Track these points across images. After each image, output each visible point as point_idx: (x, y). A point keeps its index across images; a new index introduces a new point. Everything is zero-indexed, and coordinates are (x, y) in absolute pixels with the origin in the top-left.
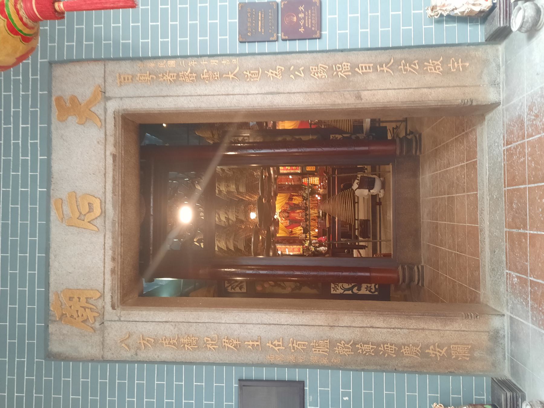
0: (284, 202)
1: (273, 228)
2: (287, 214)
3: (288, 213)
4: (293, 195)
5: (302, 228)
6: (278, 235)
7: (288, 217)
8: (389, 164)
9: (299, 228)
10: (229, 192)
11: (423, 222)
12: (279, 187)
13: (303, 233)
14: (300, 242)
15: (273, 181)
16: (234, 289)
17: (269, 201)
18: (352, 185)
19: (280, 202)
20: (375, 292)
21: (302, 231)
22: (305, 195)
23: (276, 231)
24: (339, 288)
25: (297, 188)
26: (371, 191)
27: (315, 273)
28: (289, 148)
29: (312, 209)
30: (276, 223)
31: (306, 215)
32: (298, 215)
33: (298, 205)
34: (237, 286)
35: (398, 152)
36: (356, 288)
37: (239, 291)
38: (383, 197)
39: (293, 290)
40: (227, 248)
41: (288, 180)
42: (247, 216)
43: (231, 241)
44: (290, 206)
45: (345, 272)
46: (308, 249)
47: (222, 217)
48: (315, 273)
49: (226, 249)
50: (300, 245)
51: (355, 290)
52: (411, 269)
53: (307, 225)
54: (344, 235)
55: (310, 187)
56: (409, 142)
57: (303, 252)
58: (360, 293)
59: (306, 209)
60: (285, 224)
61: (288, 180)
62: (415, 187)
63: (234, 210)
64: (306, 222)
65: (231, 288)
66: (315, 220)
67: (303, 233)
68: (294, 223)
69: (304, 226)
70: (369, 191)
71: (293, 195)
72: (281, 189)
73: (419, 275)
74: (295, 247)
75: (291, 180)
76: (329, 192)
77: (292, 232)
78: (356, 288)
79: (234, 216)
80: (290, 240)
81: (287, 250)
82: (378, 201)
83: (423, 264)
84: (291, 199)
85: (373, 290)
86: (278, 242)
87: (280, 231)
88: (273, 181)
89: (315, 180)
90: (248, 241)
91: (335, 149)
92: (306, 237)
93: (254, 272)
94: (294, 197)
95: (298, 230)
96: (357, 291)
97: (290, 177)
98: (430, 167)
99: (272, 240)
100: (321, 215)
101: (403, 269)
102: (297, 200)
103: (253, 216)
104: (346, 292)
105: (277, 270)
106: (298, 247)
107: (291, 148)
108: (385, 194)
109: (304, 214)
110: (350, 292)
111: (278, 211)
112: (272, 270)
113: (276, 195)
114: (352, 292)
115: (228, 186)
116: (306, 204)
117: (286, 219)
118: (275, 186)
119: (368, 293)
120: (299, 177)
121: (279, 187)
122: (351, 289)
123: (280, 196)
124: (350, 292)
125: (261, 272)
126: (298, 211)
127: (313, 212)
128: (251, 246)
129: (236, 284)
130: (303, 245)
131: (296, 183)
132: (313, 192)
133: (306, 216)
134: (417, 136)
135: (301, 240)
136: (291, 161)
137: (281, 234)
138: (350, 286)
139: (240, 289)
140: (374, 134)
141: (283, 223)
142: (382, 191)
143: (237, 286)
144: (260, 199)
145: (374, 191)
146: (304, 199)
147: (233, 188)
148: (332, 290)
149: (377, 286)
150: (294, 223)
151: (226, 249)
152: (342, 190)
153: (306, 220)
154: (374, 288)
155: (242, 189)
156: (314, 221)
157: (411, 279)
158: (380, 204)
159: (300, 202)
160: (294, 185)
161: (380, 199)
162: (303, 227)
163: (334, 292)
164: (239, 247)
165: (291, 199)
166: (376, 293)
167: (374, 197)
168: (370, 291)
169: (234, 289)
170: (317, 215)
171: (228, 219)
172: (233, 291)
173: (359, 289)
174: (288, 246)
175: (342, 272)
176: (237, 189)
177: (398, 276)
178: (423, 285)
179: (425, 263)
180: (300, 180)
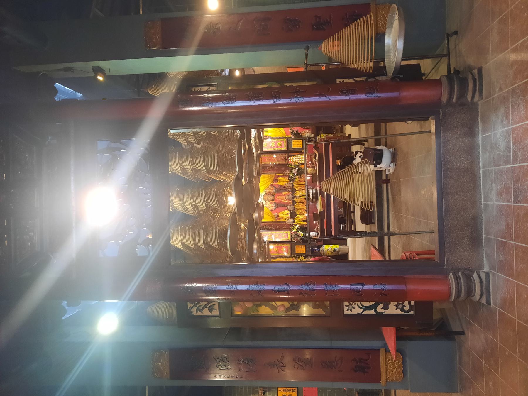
0: (269, 183)
1: (257, 215)
2: (272, 197)
3: (273, 195)
4: (278, 176)
5: (289, 212)
6: (263, 221)
7: (273, 200)
8: (427, 119)
9: (287, 212)
10: (195, 171)
11: (486, 206)
12: (263, 168)
13: (291, 217)
14: (289, 228)
15: (255, 158)
16: (201, 310)
17: (250, 182)
18: (354, 159)
19: (264, 184)
20: (409, 311)
21: (289, 215)
22: (291, 175)
23: (261, 217)
24: (356, 306)
25: (285, 167)
26: (378, 166)
27: (322, 287)
28: (276, 97)
29: (299, 190)
30: (260, 208)
31: (294, 197)
32: (285, 198)
33: (284, 187)
34: (205, 306)
35: (445, 99)
36: (381, 305)
37: (209, 313)
38: (393, 173)
39: (287, 310)
40: (195, 245)
41: (272, 159)
42: (222, 202)
43: (201, 237)
44: (275, 188)
45: (367, 284)
46: (296, 235)
47: (180, 203)
48: (322, 287)
49: (193, 247)
50: (287, 230)
51: (380, 309)
52: (468, 278)
53: (294, 209)
54: (341, 220)
55: (298, 166)
56: (463, 83)
57: (292, 238)
58: (387, 312)
59: (293, 191)
60: (270, 208)
61: (272, 159)
62: (472, 151)
63: (203, 195)
64: (293, 205)
65: (197, 310)
66: (303, 203)
67: (291, 217)
68: (280, 205)
69: (291, 209)
70: (375, 166)
71: (278, 176)
72: (265, 169)
73: (482, 287)
74: (282, 232)
75: (275, 160)
76: (321, 171)
77: (278, 216)
78: (381, 305)
79: (204, 202)
80: (277, 225)
81: (273, 236)
82: (384, 178)
83: (486, 269)
84: (276, 180)
85: (407, 309)
86: (263, 228)
87: (265, 216)
88: (255, 158)
89: (300, 158)
90: (223, 235)
91: (347, 98)
92: (294, 222)
93: (229, 288)
94: (279, 178)
95: (285, 214)
96: (383, 311)
97: (275, 156)
98: (507, 117)
99: (255, 227)
100: (311, 197)
101: (457, 278)
102: (283, 181)
103: (232, 200)
104: (367, 312)
105: (263, 284)
106: (286, 232)
107: (279, 98)
108: (395, 169)
109: (291, 196)
110: (372, 312)
111: (262, 193)
112: (256, 283)
113: (259, 175)
114: (376, 311)
115: (192, 163)
116: (293, 185)
117: (271, 203)
118: (258, 164)
119: (399, 312)
120: (284, 155)
121: (263, 168)
122: (374, 307)
123: (264, 178)
124: (372, 312)
125: (240, 287)
126: (284, 193)
127: (300, 194)
128: (227, 243)
129: (205, 303)
130: (291, 230)
131: (281, 163)
132: (301, 172)
133: (293, 198)
134: (475, 71)
135: (288, 225)
136: (279, 118)
137: (267, 219)
138: (372, 303)
139: (210, 310)
140: (402, 76)
141: (268, 207)
142: (392, 165)
143: (205, 306)
144: (238, 179)
145: (382, 166)
146: (291, 179)
147: (201, 165)
148: (346, 309)
149: (412, 303)
150: (280, 205)
151: (193, 247)
152: (341, 167)
153: (294, 203)
154: (408, 306)
155: (213, 166)
156: (302, 204)
157: (470, 292)
158: (387, 181)
159: (286, 183)
160: (279, 165)
161: (387, 175)
162: (290, 211)
163: (349, 312)
164: (211, 244)
165: (276, 180)
166: (412, 313)
167: (379, 174)
168: (402, 310)
169: (201, 310)
170: (305, 197)
171: (195, 207)
172: (199, 313)
173: (386, 308)
174: (274, 232)
175: (363, 284)
176: (207, 166)
177: (450, 289)
178: (488, 303)
179: (492, 267)
180: (285, 159)
